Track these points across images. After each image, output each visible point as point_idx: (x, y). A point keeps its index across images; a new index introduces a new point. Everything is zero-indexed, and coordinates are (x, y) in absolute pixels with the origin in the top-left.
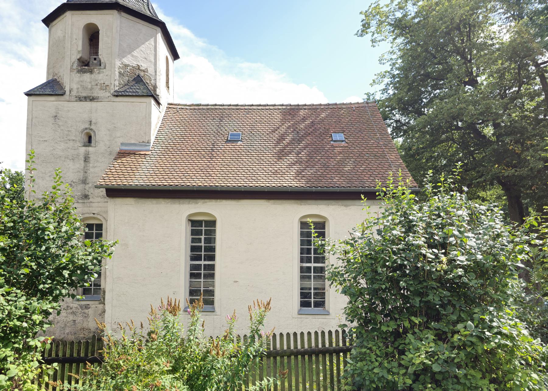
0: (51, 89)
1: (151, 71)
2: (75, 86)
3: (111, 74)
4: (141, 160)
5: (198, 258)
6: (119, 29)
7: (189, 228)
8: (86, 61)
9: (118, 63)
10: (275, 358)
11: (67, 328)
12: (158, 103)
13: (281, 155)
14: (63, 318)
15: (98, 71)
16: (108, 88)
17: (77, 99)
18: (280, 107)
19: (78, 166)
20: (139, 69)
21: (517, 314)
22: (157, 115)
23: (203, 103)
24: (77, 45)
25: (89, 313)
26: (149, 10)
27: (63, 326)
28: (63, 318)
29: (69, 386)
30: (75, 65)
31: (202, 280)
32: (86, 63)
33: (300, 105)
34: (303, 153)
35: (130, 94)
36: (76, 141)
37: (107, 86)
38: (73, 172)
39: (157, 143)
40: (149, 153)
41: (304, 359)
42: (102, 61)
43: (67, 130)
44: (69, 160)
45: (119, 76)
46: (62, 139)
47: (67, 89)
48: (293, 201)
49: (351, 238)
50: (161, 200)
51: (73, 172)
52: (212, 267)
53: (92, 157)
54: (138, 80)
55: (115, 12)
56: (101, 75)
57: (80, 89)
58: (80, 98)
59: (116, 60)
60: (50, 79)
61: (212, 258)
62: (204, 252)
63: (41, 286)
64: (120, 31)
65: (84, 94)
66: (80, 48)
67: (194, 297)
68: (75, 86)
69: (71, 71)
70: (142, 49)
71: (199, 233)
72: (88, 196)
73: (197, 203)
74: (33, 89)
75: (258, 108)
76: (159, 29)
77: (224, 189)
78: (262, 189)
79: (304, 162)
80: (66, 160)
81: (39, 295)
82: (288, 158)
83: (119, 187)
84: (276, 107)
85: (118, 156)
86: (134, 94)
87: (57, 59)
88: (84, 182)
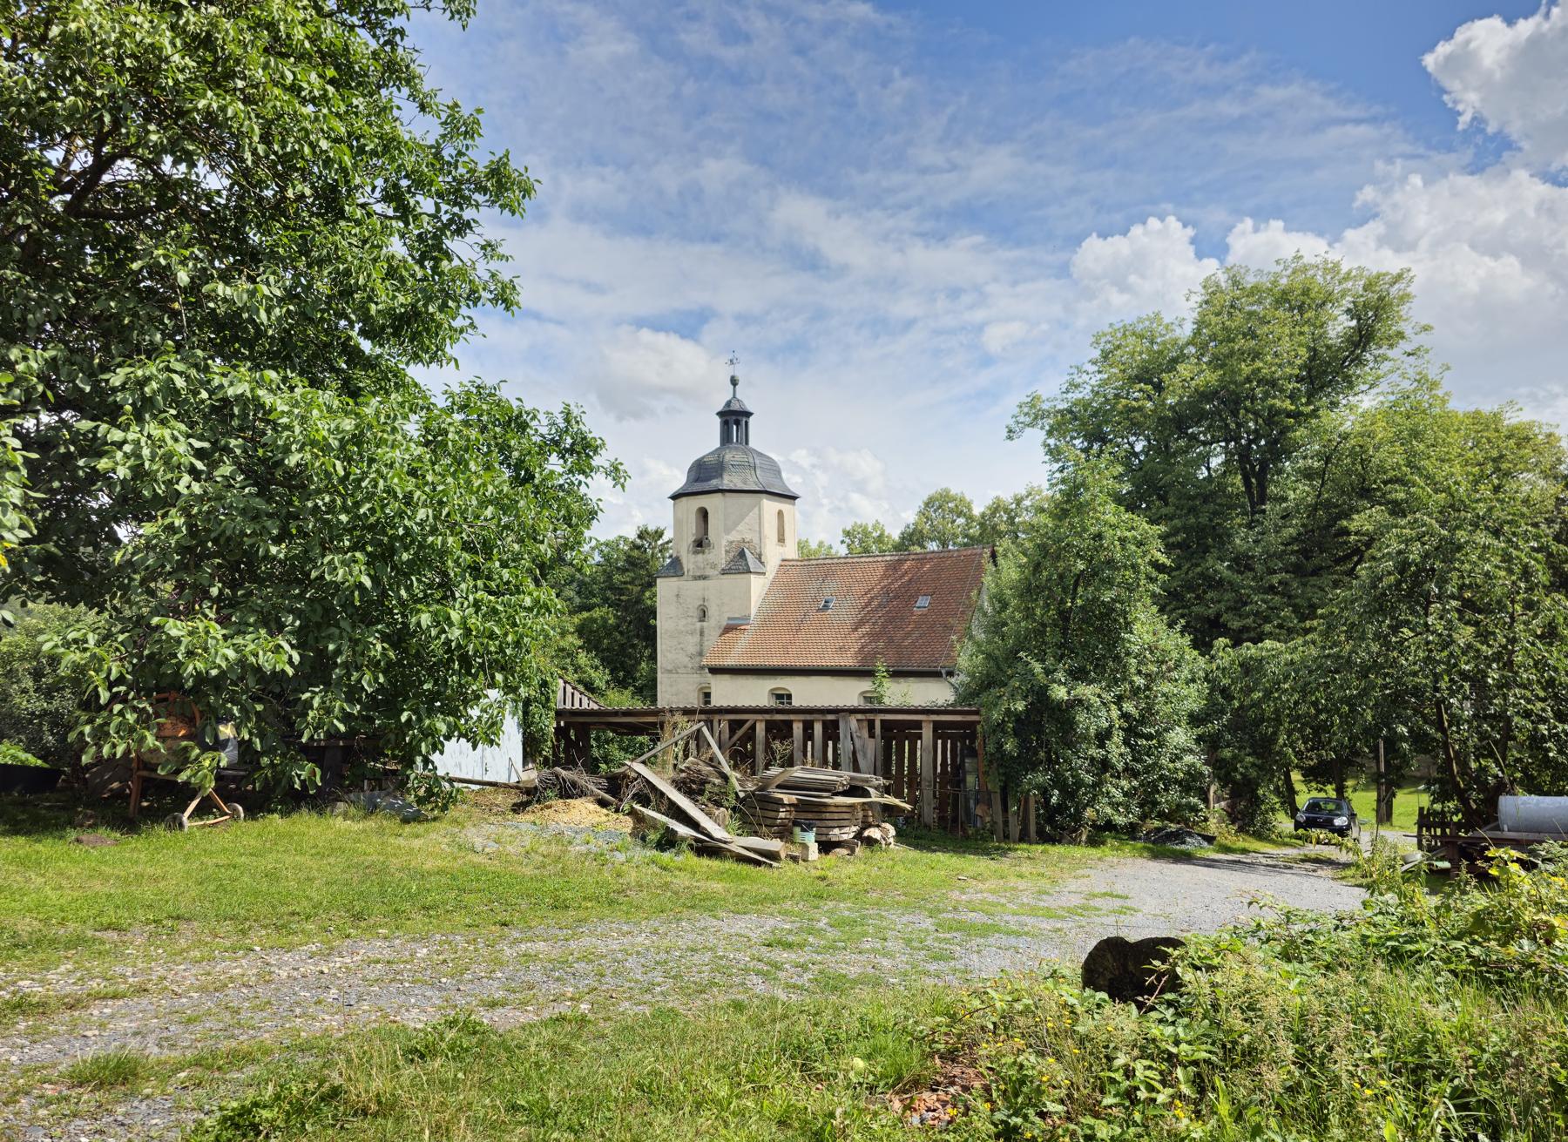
1: (756, 540)
3: (719, 554)
9: (724, 543)
21: (27, 666)
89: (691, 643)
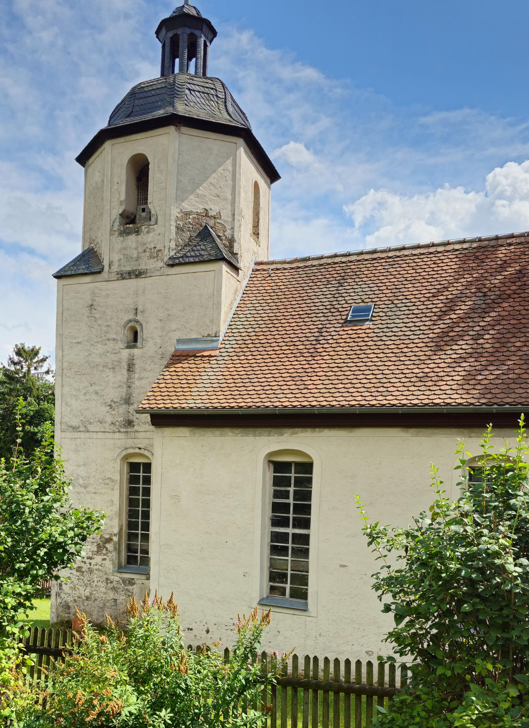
0: (87, 264)
1: (226, 216)
2: (116, 257)
3: (164, 234)
4: (202, 365)
5: (284, 522)
6: (177, 155)
7: (270, 475)
8: (132, 214)
9: (175, 212)
10: (315, 692)
11: (106, 609)
12: (236, 269)
13: (442, 342)
14: (102, 595)
15: (147, 230)
16: (160, 254)
17: (119, 276)
18: (457, 247)
19: (119, 378)
20: (207, 215)
22: (230, 287)
23: (313, 254)
24: (118, 193)
25: (134, 591)
26: (227, 111)
27: (101, 605)
28: (102, 595)
29: (31, 680)
30: (117, 224)
31: (289, 558)
32: (133, 217)
33: (501, 238)
34: (487, 337)
35: (192, 260)
36: (117, 340)
37: (160, 250)
38: (113, 388)
39: (230, 334)
40: (217, 353)
41: (360, 701)
42: (153, 212)
43: (105, 324)
44: (108, 370)
45: (177, 233)
46: (100, 339)
47: (106, 263)
48: (454, 430)
49: (416, 528)
50: (227, 431)
51: (113, 388)
52: (305, 539)
53: (138, 365)
54: (205, 234)
55: (171, 129)
56: (151, 235)
57: (122, 261)
58: (122, 274)
59: (172, 207)
60: (86, 248)
61: (306, 524)
62: (294, 513)
63: (17, 566)
64: (179, 158)
65: (128, 269)
66: (123, 197)
67: (276, 584)
68: (116, 257)
69: (111, 235)
70: (213, 181)
71: (286, 482)
72: (133, 422)
73: (282, 434)
74: (64, 267)
75: (414, 252)
76: (241, 142)
77: (325, 411)
78: (393, 410)
79: (486, 355)
80: (105, 369)
81: (16, 575)
82: (455, 347)
83: (167, 412)
84: (450, 247)
85: (172, 361)
86: (197, 260)
87: (95, 217)
88: (128, 401)
89: (112, 385)
